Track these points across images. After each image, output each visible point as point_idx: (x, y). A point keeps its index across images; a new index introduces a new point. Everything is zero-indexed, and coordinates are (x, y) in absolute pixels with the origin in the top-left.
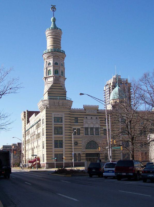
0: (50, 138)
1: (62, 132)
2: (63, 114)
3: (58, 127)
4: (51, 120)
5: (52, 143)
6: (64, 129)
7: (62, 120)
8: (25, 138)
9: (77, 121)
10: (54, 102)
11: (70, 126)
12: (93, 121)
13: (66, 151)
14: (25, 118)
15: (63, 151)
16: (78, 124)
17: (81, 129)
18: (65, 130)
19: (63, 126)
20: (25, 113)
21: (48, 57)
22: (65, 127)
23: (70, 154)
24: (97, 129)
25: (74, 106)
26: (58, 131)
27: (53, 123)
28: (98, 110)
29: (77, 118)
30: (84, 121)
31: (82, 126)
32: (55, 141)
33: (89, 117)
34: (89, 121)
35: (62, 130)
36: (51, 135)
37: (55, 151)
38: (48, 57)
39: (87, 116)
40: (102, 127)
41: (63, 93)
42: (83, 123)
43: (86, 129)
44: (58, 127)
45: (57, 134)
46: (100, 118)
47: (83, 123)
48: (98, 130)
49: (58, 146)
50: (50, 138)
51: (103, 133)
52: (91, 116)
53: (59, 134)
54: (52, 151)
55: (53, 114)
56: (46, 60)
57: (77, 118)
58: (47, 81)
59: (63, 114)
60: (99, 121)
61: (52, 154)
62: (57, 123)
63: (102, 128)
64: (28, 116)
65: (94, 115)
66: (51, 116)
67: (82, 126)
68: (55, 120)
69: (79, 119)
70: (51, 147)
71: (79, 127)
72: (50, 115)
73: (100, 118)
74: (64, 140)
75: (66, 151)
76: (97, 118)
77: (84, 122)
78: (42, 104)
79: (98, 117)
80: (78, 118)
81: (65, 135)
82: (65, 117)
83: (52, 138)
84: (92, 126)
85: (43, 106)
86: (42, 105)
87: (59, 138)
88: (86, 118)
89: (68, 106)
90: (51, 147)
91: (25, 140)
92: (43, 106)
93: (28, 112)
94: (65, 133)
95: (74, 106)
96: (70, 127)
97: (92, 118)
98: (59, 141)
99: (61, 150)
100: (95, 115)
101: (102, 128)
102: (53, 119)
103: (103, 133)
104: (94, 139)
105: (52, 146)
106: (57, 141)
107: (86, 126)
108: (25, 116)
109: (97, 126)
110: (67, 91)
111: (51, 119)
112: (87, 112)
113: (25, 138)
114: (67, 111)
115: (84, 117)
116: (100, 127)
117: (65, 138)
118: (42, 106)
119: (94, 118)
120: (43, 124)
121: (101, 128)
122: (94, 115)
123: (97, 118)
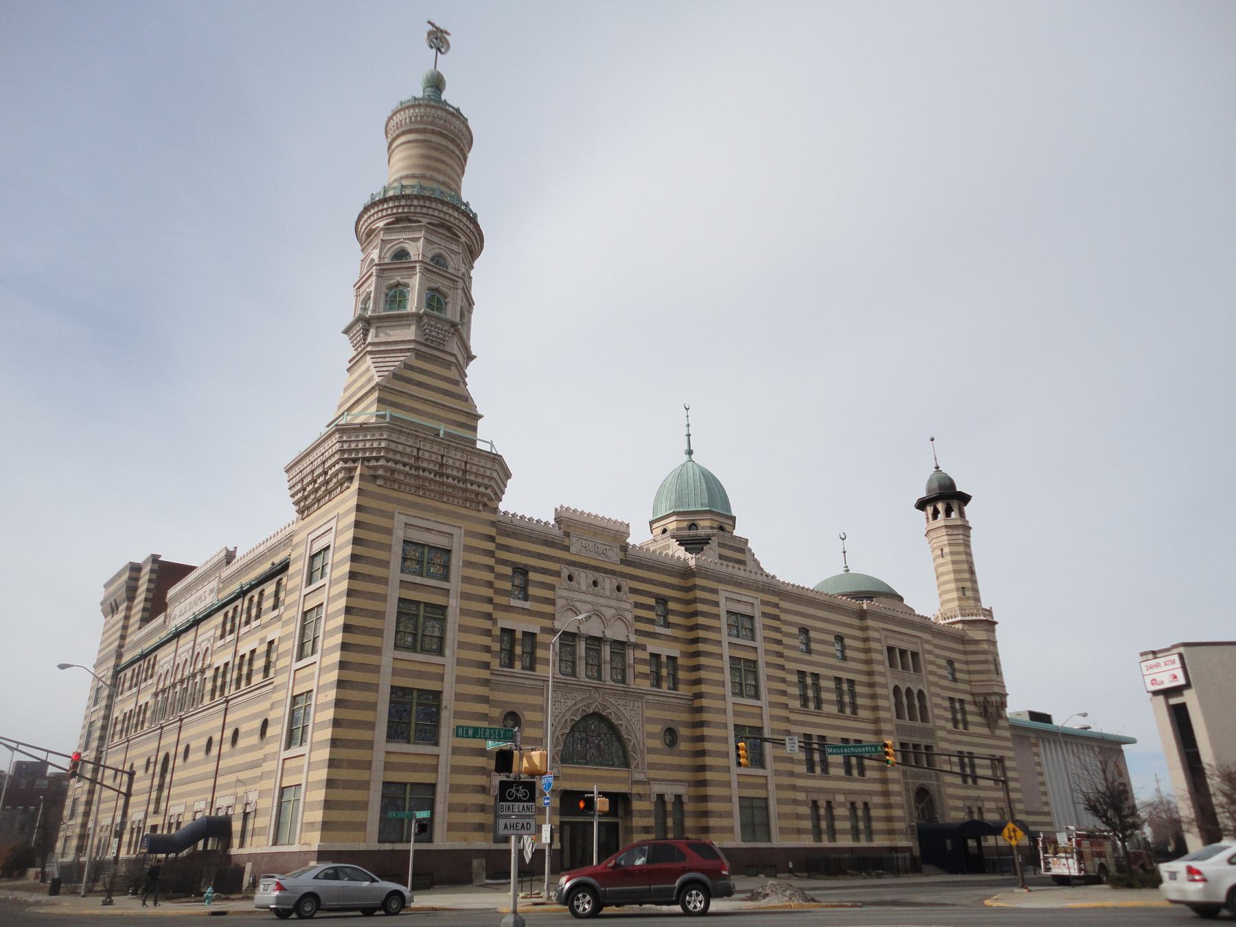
0: (362, 667)
1: (441, 639)
2: (455, 531)
3: (422, 607)
4: (381, 555)
5: (372, 706)
6: (453, 619)
7: (446, 567)
8: (109, 707)
9: (524, 589)
10: (418, 449)
11: (488, 608)
12: (603, 601)
13: (455, 769)
14: (131, 598)
15: (435, 769)
16: (527, 605)
17: (541, 638)
18: (463, 629)
19: (454, 604)
20: (134, 575)
21: (397, 221)
22: (464, 612)
23: (477, 792)
24: (620, 646)
25: (514, 502)
26: (420, 625)
27: (395, 573)
28: (624, 548)
29: (522, 571)
30: (560, 592)
31: (547, 623)
32: (395, 690)
33: (584, 578)
34: (583, 597)
35: (443, 630)
36: (377, 650)
37: (388, 766)
38: (397, 221)
39: (576, 572)
40: (642, 640)
41: (461, 419)
42: (552, 602)
43: (569, 638)
44: (422, 607)
45: (413, 649)
46: (633, 591)
47: (552, 602)
48: (623, 656)
49: (413, 725)
50: (362, 667)
51: (645, 676)
52: (592, 575)
53: (424, 651)
54: (368, 765)
55: (399, 520)
56: (381, 236)
57: (522, 571)
58: (369, 340)
59: (455, 531)
60: (629, 606)
61: (365, 785)
62: (418, 580)
63: (643, 648)
64: (154, 576)
65: (606, 571)
66: (389, 531)
67: (547, 623)
68: (404, 559)
69: (532, 576)
70: (363, 735)
71: (533, 626)
72: (383, 522)
73: (633, 591)
74: (449, 690)
75: (455, 769)
76: (619, 589)
77: (560, 602)
78: (338, 446)
79: (627, 584)
80: (527, 573)
81: (460, 662)
82: (468, 549)
83: (376, 669)
84: (594, 629)
85: (341, 464)
86: (337, 457)
87: (420, 675)
88: (570, 578)
89: (489, 491)
90: (363, 735)
91: (106, 718)
92: (341, 464)
93: (156, 567)
94: (462, 645)
95: (514, 502)
96: (489, 616)
97: (595, 583)
98: (419, 696)
99: (429, 761)
100: (613, 573)
101: (643, 648)
102: (398, 550)
103: (645, 676)
104: (605, 707)
105: (371, 726)
106: (406, 691)
107: (565, 623)
108: (135, 589)
109: (617, 632)
110: (480, 411)
111: (388, 547)
112: (573, 549)
113: (109, 707)
114: (478, 521)
115: (558, 574)
116: (633, 638)
117: (460, 680)
118: (337, 462)
119: (608, 583)
120: (310, 581)
121: (636, 646)
122: (606, 571)
123: (619, 589)
